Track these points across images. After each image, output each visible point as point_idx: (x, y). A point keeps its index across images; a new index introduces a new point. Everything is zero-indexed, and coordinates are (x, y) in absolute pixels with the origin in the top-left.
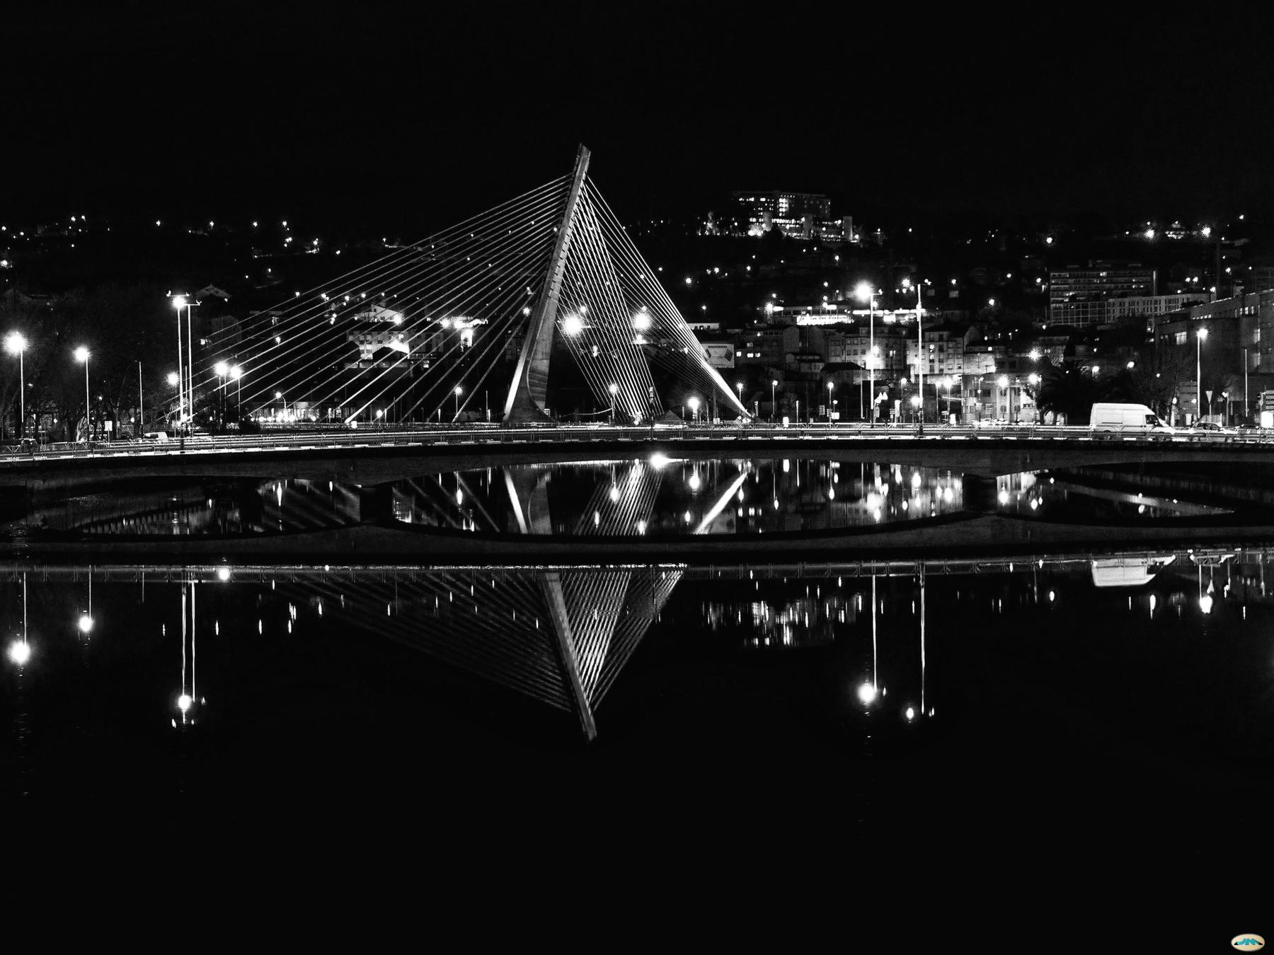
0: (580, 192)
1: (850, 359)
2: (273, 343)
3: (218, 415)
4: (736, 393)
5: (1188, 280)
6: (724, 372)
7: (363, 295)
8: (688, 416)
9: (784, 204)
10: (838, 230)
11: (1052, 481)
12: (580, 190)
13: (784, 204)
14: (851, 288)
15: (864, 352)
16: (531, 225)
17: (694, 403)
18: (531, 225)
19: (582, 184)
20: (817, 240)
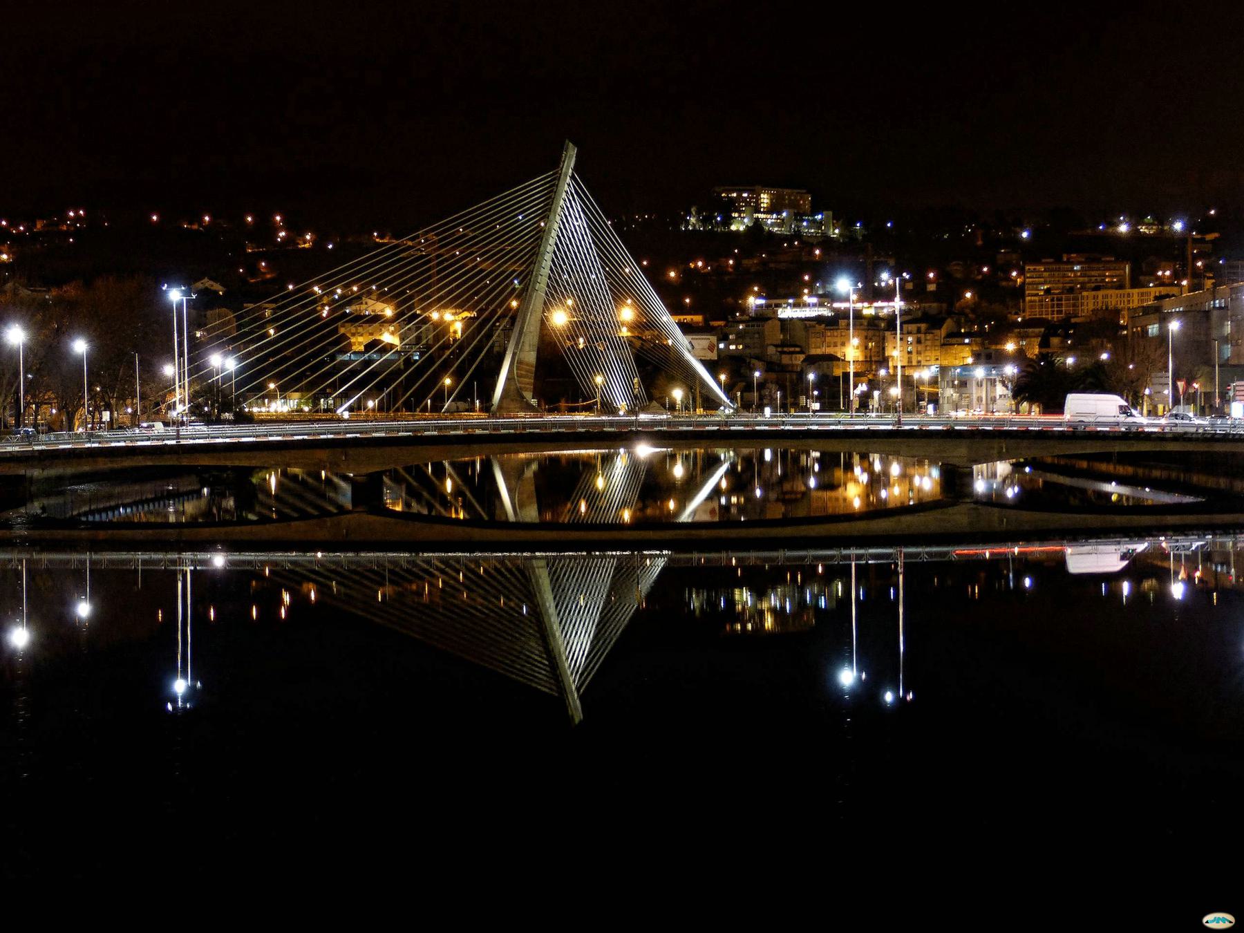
0: (566, 188)
4: (719, 383)
12: (567, 185)
15: (843, 344)
17: (678, 394)
18: (487, 285)
19: (568, 180)
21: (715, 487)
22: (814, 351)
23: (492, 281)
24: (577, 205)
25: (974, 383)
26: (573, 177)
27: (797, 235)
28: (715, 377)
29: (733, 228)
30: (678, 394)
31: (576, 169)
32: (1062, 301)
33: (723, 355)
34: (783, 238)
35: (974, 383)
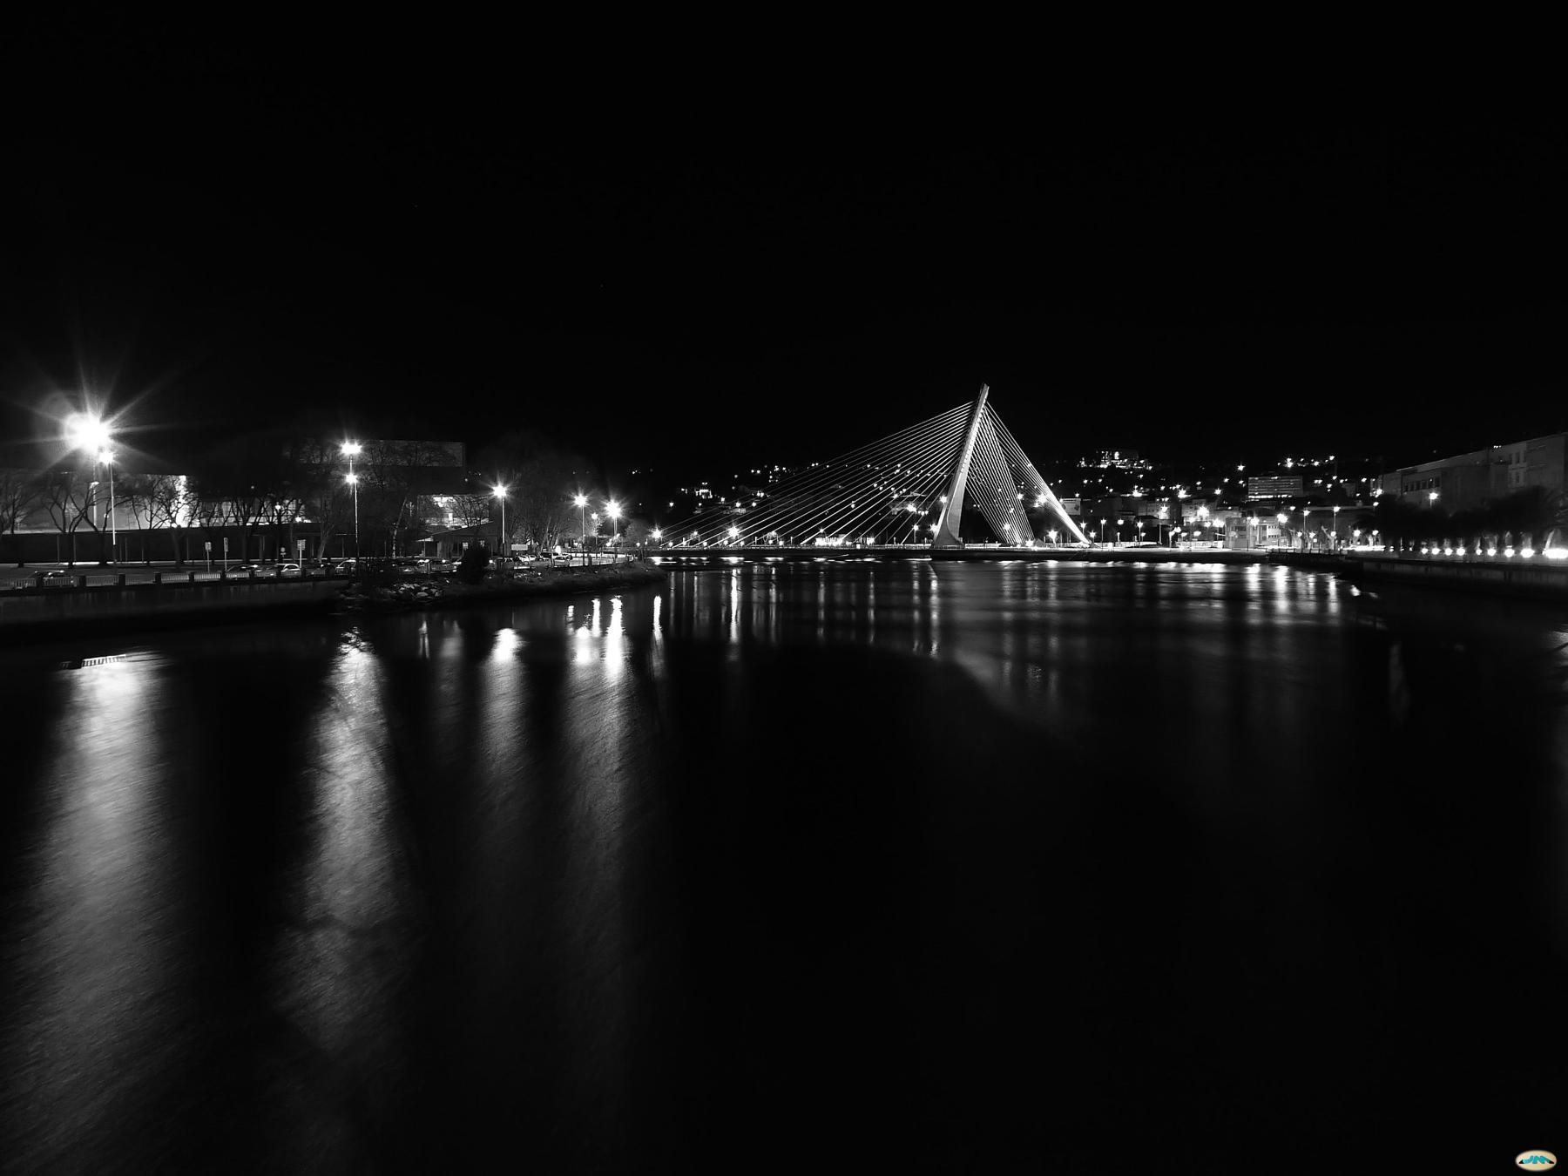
0: (982, 411)
1: (1149, 514)
2: (912, 470)
3: (236, 516)
4: (1081, 529)
5: (813, 465)
6: (1073, 517)
7: (869, 466)
8: (1049, 541)
9: (1117, 454)
10: (1141, 465)
11: (1121, 522)
12: (982, 410)
13: (1117, 454)
14: (352, 438)
15: (1158, 511)
16: (927, 477)
17: (1053, 534)
18: (927, 477)
19: (983, 406)
20: (1132, 469)
21: (1073, 519)
22: (1140, 514)
23: (932, 474)
24: (990, 422)
25: (1251, 529)
26: (986, 404)
27: (1132, 469)
28: (1078, 525)
29: (1102, 466)
30: (1053, 534)
31: (987, 400)
32: (716, 555)
33: (675, 536)
34: (1124, 470)
35: (1251, 529)
